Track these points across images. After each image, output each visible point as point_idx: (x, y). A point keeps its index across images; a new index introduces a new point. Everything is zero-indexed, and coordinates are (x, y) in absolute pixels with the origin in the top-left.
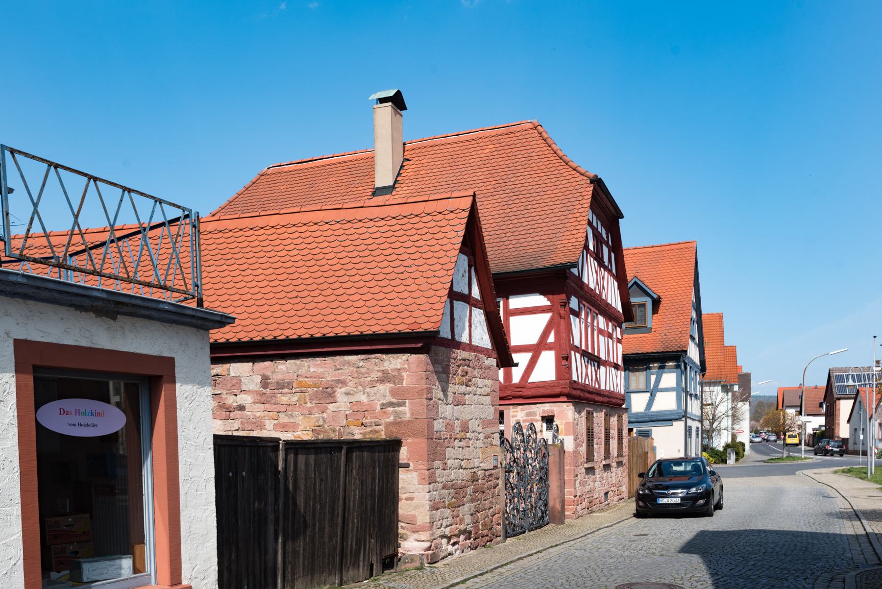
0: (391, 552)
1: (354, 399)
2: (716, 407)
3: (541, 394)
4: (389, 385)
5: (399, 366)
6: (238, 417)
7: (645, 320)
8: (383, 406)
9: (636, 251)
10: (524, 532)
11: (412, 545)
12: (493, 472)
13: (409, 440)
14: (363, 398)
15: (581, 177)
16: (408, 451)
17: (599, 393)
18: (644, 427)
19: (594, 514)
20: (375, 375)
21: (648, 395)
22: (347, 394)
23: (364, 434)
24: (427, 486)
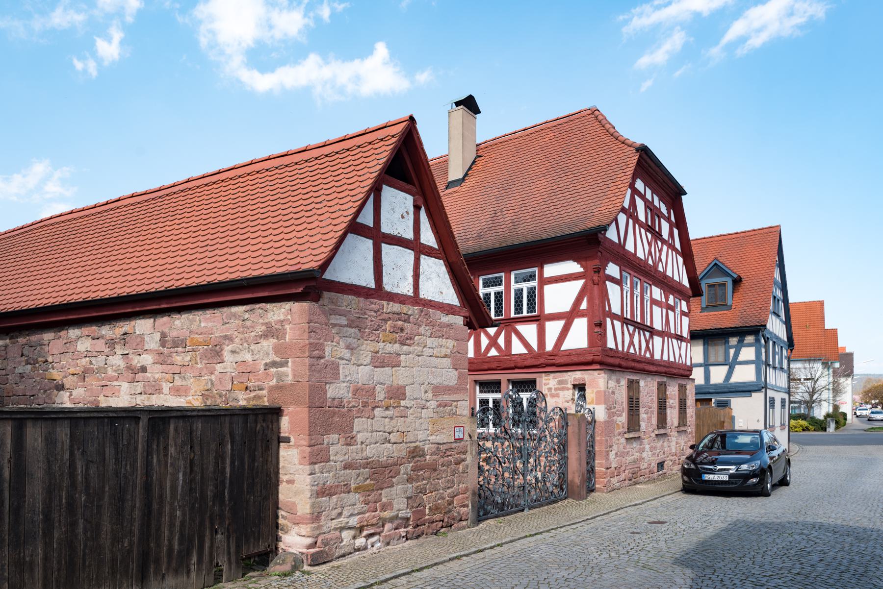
0: (262, 548)
1: (239, 358)
2: (816, 382)
3: (567, 362)
4: (273, 341)
5: (282, 317)
6: (141, 379)
7: (725, 299)
8: (267, 366)
9: (720, 238)
10: (523, 510)
11: (294, 540)
12: (454, 445)
13: (291, 409)
14: (248, 357)
15: (629, 148)
16: (290, 422)
17: (652, 362)
18: (722, 398)
19: (638, 486)
20: (260, 329)
21: (726, 368)
22: (233, 352)
23: (248, 400)
24: (308, 467)
